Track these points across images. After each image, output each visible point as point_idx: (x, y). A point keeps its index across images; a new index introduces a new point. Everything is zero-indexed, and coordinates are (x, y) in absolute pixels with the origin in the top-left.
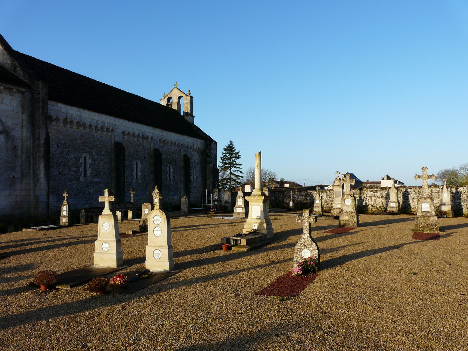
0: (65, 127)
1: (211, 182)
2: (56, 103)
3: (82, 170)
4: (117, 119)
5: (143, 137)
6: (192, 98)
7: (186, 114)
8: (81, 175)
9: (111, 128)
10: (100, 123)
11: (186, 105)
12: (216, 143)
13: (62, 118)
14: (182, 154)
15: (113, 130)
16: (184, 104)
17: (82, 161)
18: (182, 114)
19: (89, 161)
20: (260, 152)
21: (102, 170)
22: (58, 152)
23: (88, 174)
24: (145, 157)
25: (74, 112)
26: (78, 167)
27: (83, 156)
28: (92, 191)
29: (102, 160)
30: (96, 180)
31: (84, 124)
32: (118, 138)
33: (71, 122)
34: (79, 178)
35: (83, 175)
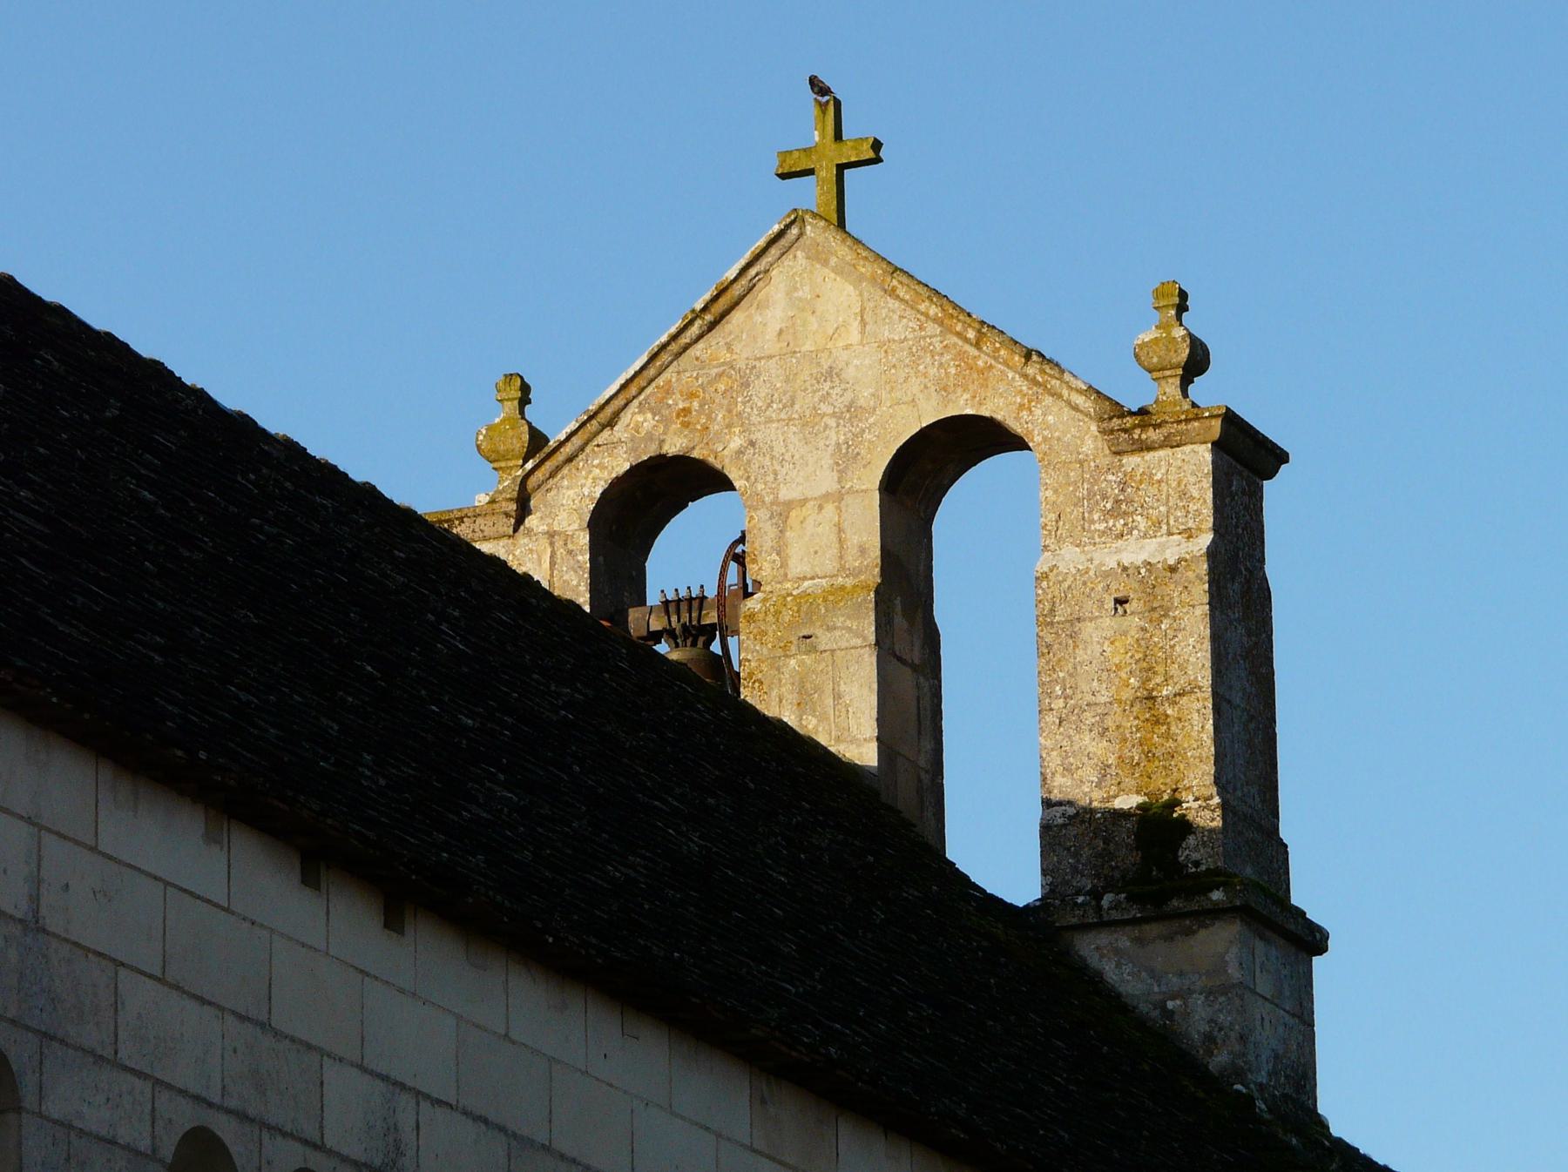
6: (1246, 458)
7: (1128, 861)
11: (1103, 639)
16: (1055, 627)
18: (997, 854)
20: (814, 82)
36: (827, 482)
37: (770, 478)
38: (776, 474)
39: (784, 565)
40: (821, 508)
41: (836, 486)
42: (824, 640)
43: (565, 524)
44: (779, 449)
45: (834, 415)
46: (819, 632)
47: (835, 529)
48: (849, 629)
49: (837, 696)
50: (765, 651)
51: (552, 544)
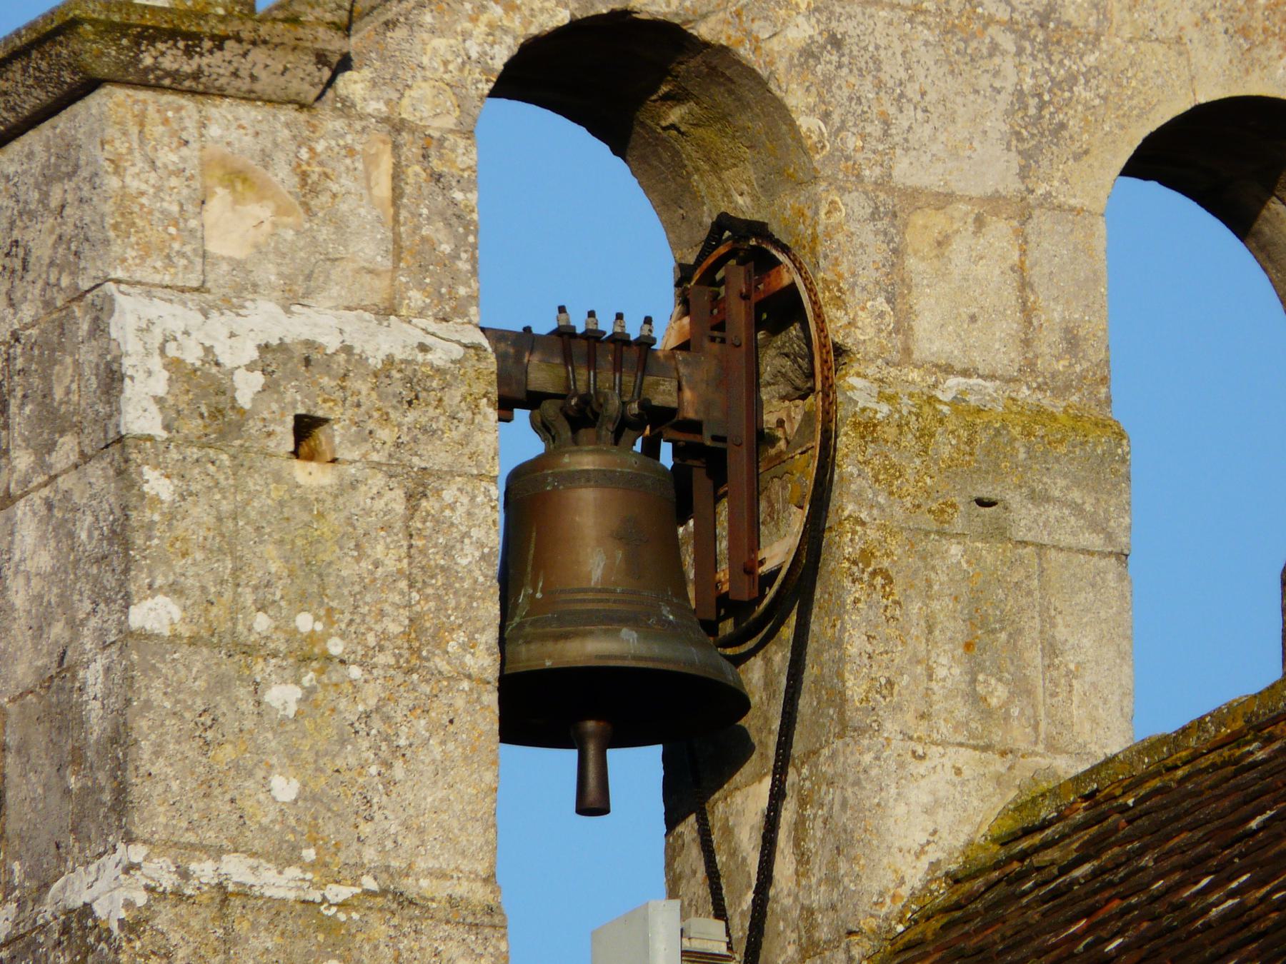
36: (995, 170)
37: (875, 129)
38: (887, 123)
39: (903, 327)
40: (980, 222)
41: (1012, 186)
42: (1025, 518)
43: (426, 110)
44: (893, 70)
45: (1010, 26)
46: (1015, 499)
47: (1013, 278)
48: (1078, 509)
49: (1052, 649)
50: (899, 513)
51: (396, 147)
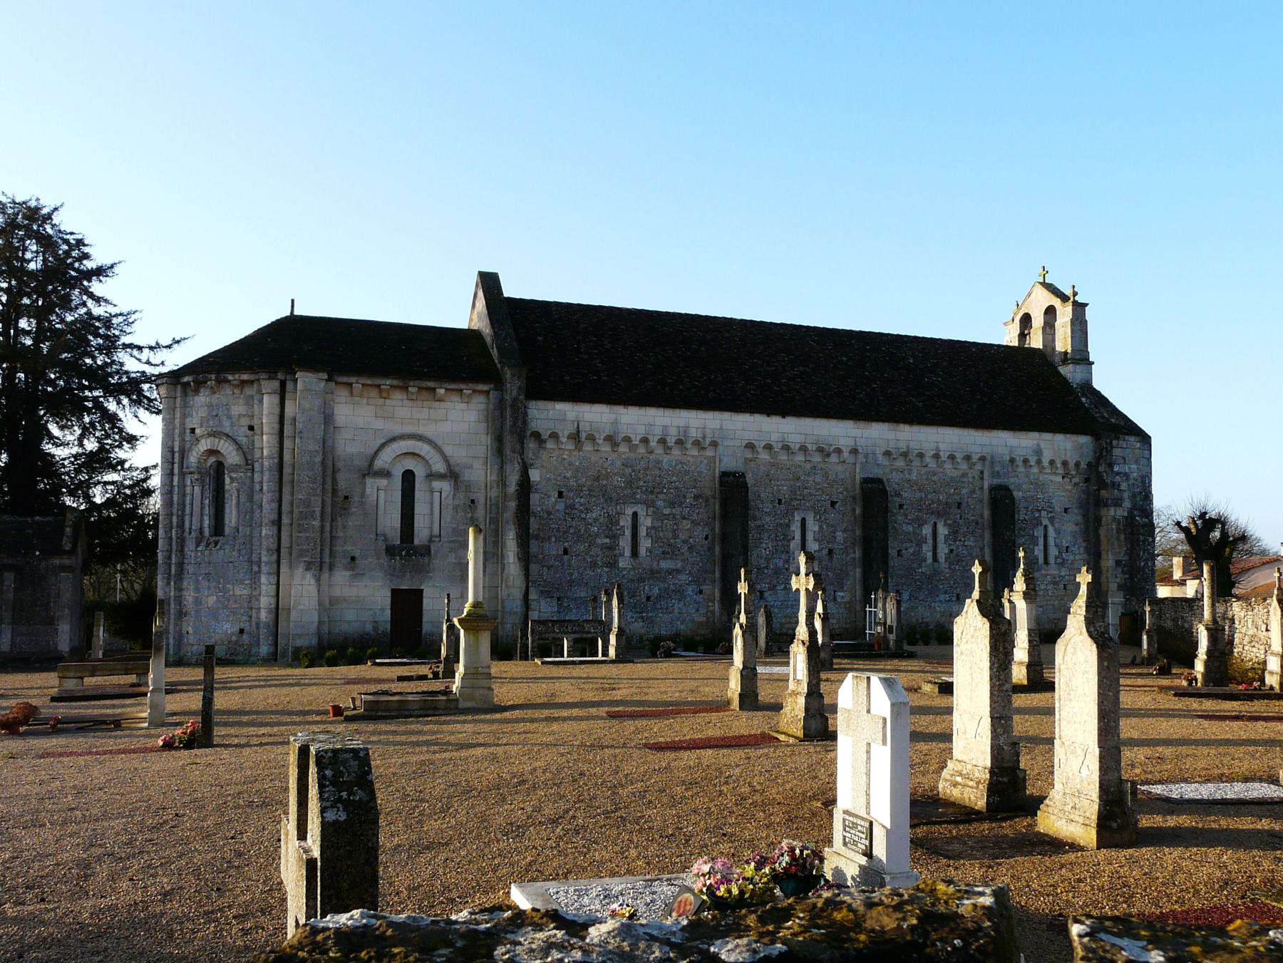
0: (580, 450)
1: (1118, 563)
2: (549, 405)
3: (625, 543)
4: (726, 415)
5: (820, 450)
8: (622, 555)
9: (708, 441)
10: (673, 431)
12: (1145, 439)
13: (566, 433)
14: (986, 486)
15: (714, 444)
17: (626, 522)
19: (646, 522)
21: (685, 542)
22: (561, 506)
23: (642, 551)
24: (833, 504)
25: (596, 415)
26: (614, 537)
27: (629, 511)
28: (656, 591)
29: (684, 518)
30: (665, 565)
31: (628, 440)
32: (730, 462)
33: (591, 438)
34: (616, 562)
35: (627, 553)
